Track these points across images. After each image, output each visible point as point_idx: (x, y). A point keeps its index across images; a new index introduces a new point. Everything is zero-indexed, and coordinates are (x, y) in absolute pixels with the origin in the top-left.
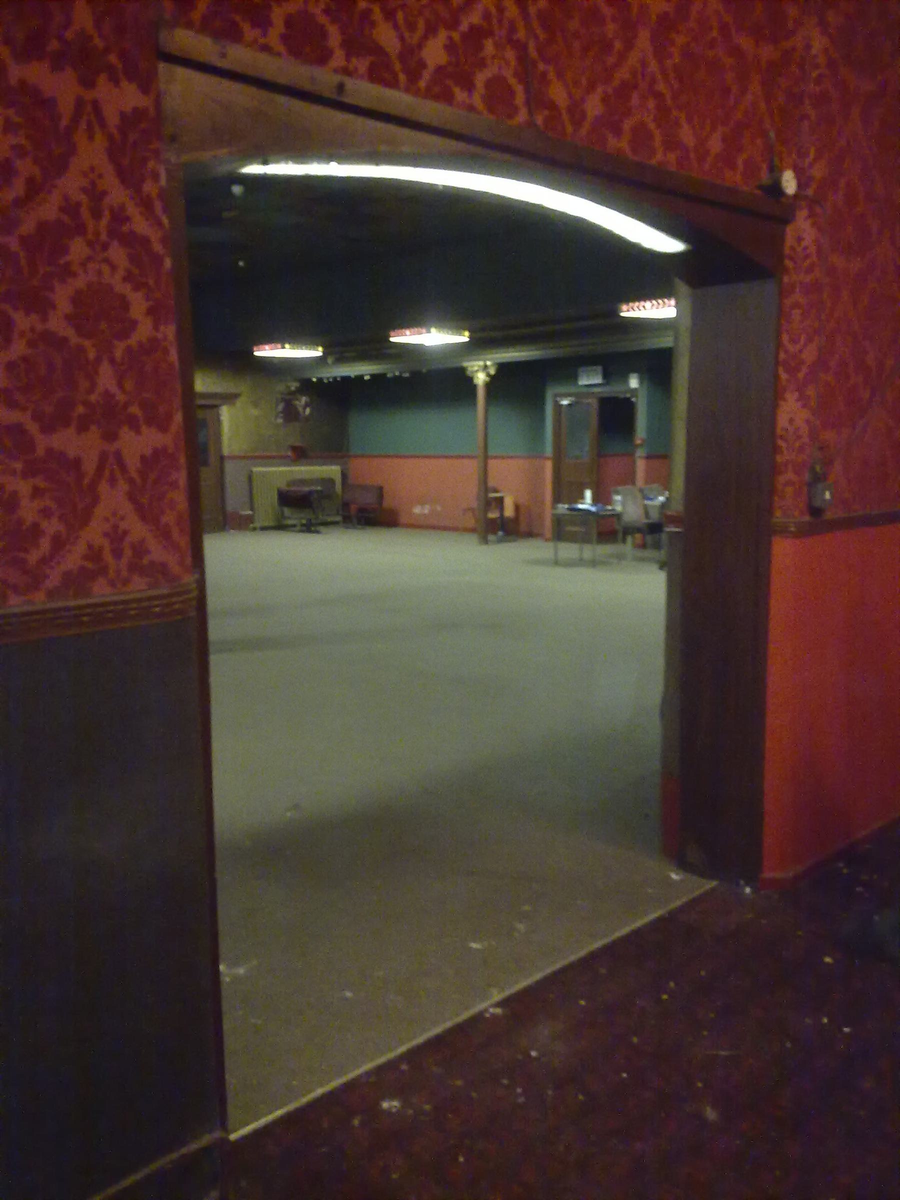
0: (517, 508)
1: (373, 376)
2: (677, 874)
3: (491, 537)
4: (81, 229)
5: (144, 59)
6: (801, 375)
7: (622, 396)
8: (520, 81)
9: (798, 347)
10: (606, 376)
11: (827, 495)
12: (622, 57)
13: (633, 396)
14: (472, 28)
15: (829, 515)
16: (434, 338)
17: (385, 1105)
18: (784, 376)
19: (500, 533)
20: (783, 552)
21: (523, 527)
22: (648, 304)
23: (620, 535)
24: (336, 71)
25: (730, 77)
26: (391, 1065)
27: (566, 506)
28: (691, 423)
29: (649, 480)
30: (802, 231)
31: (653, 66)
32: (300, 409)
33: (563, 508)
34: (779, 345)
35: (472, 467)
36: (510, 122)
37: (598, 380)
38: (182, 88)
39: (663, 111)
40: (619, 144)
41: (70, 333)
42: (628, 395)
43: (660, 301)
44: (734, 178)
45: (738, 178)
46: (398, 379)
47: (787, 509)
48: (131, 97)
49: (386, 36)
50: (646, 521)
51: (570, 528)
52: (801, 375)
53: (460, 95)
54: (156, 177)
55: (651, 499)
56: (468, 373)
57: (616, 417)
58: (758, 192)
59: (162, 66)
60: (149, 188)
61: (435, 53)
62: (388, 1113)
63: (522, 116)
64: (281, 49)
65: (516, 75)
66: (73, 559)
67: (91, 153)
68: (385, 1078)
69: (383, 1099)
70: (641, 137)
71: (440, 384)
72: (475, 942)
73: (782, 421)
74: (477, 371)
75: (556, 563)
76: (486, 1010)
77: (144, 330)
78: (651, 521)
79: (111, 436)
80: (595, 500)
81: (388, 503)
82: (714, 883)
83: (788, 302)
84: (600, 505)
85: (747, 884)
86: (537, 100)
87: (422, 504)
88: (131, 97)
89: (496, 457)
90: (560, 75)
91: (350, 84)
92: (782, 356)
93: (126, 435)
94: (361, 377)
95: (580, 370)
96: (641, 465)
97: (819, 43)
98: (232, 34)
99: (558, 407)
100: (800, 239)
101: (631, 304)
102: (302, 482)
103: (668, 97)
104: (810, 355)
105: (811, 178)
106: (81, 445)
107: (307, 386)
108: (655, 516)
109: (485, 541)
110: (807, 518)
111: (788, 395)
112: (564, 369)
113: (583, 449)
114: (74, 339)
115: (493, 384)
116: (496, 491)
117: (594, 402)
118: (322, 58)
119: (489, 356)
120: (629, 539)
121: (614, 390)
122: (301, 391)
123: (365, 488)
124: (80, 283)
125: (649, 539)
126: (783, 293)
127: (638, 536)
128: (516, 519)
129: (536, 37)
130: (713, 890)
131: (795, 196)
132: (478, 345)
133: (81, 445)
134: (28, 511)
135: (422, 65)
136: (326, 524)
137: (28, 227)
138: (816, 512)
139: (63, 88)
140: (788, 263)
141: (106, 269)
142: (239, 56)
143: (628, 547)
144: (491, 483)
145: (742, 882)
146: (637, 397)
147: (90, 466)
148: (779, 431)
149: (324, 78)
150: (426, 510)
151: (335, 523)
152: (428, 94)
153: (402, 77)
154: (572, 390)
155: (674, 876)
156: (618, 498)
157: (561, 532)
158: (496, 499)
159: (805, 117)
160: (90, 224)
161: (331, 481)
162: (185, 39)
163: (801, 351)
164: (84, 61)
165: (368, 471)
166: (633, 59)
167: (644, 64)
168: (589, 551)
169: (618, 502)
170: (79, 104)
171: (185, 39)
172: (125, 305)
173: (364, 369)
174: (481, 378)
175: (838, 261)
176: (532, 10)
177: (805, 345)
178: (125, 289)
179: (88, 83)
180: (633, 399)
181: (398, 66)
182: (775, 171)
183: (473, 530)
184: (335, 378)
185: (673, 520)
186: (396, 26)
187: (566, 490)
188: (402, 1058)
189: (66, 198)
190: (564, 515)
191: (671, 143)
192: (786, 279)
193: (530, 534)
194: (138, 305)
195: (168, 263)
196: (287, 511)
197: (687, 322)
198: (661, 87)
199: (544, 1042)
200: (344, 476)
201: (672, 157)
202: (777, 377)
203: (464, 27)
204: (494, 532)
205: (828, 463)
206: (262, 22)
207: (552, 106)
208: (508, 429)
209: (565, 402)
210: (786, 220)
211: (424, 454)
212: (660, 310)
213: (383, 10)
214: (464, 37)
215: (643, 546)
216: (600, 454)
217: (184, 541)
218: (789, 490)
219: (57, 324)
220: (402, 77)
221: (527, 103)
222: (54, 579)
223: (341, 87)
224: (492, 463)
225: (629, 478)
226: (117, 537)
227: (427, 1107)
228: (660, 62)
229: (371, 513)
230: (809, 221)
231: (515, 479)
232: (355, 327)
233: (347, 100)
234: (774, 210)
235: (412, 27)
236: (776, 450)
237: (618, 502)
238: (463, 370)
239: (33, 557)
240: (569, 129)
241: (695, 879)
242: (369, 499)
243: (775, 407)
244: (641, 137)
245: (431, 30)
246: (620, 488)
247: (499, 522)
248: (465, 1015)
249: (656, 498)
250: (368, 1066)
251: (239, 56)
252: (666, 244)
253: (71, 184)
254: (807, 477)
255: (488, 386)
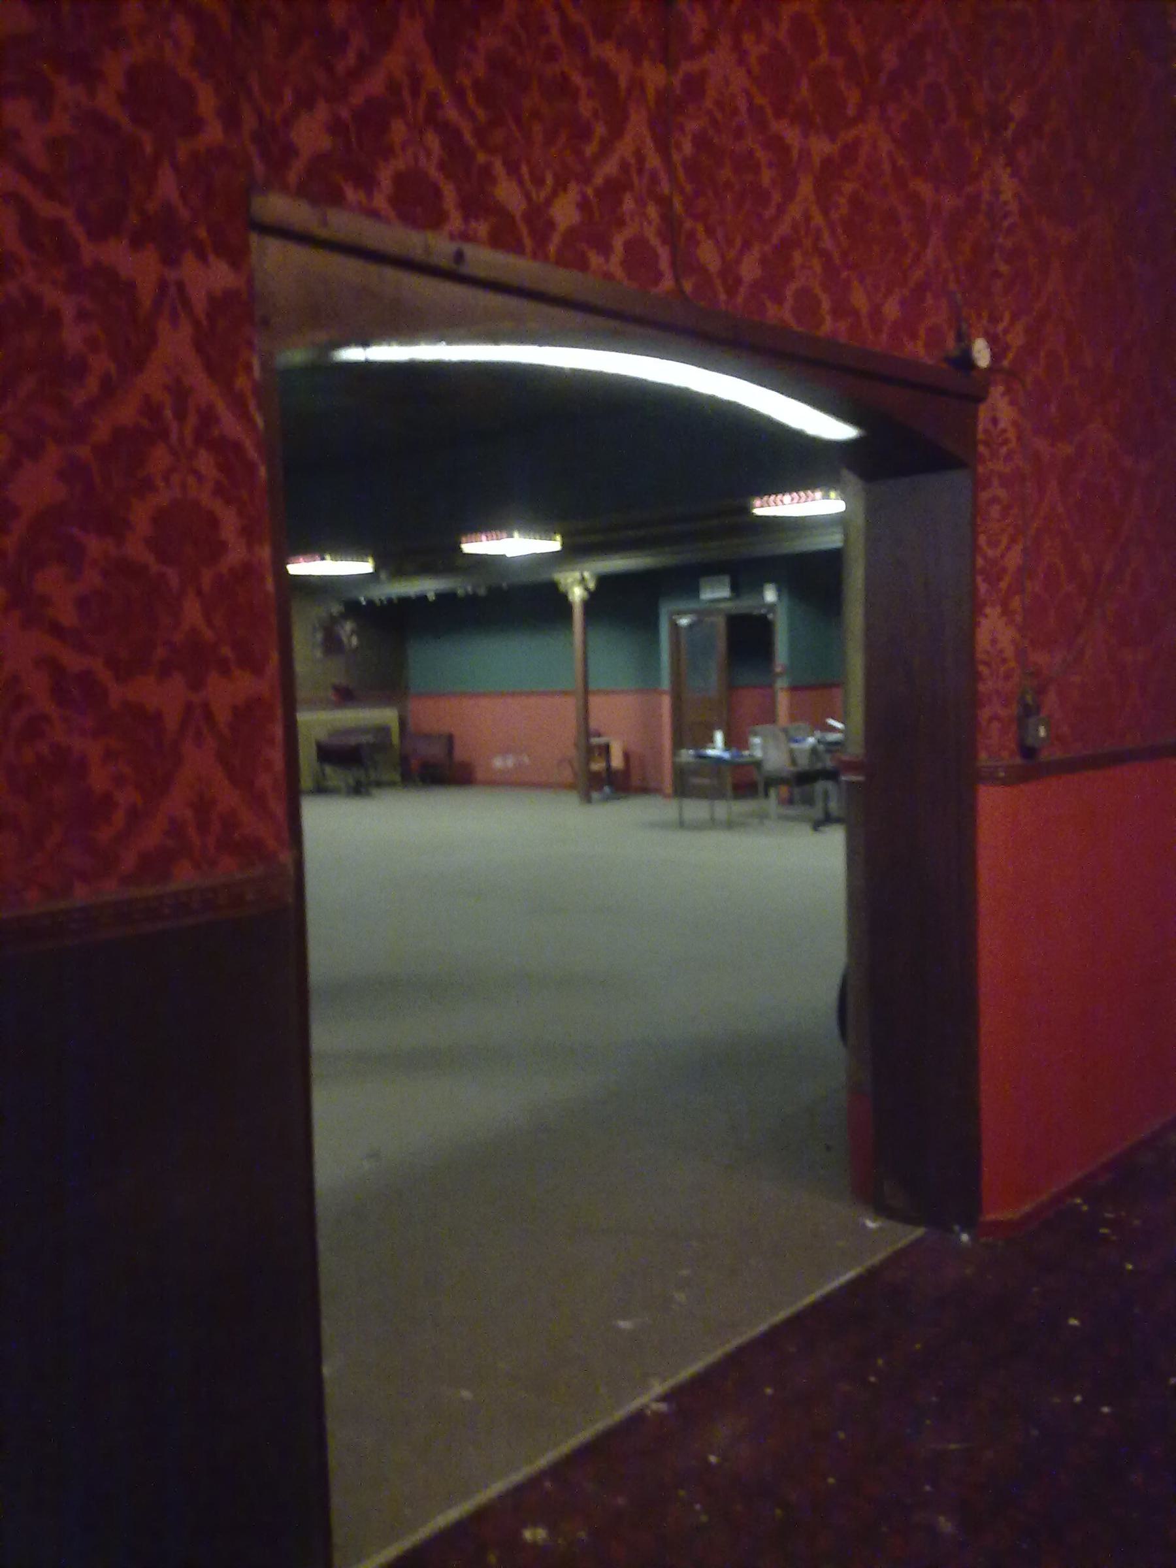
0: (627, 756)
1: (440, 596)
2: (874, 1221)
3: (595, 795)
4: (164, 434)
5: (233, 230)
6: (1003, 585)
7: (756, 612)
8: (664, 242)
9: (998, 552)
10: (736, 588)
11: (1042, 732)
12: (781, 209)
13: (769, 612)
14: (608, 181)
15: (1045, 756)
16: (516, 545)
17: (528, 1535)
18: (983, 587)
19: (607, 789)
20: (991, 800)
21: (635, 780)
22: (787, 498)
23: (761, 788)
24: (452, 237)
25: (907, 228)
26: (533, 1482)
27: (691, 752)
28: (871, 648)
29: (793, 718)
30: (999, 410)
31: (818, 219)
32: (345, 639)
33: (687, 755)
34: (975, 548)
35: (569, 707)
36: (654, 291)
37: (724, 592)
38: (274, 259)
39: (670, 229)
40: (781, 313)
41: (149, 559)
42: (763, 611)
43: (802, 494)
44: (917, 350)
45: (788, 316)
46: (472, 599)
47: (994, 748)
48: (219, 276)
49: (507, 193)
50: (792, 769)
51: (697, 781)
52: (1003, 585)
53: (595, 259)
54: (248, 368)
55: (796, 741)
56: (562, 588)
57: (748, 639)
58: (944, 366)
59: (254, 238)
60: (241, 382)
61: (565, 212)
62: (534, 1545)
63: (668, 283)
64: (392, 214)
65: (659, 233)
66: (152, 836)
67: (175, 343)
68: (522, 1502)
69: (525, 1525)
70: (806, 305)
71: (527, 601)
72: (624, 1319)
73: (983, 638)
74: (573, 584)
75: (682, 825)
76: (647, 1406)
77: (236, 554)
78: (799, 769)
79: (196, 684)
80: (728, 744)
81: (459, 754)
82: (920, 1232)
83: (985, 496)
84: (734, 750)
85: (963, 1230)
86: (685, 264)
87: (505, 751)
88: (219, 276)
89: (607, 693)
90: (710, 231)
91: (469, 250)
92: (980, 562)
93: (189, 260)
94: (422, 599)
95: (703, 581)
96: (783, 700)
97: (1009, 187)
98: (335, 198)
99: (675, 627)
100: (995, 421)
101: (766, 498)
102: (348, 732)
103: (836, 255)
104: (1014, 559)
105: (1007, 348)
106: (165, 696)
107: (353, 609)
108: (804, 763)
109: (587, 799)
110: (1018, 760)
111: (988, 610)
112: (684, 581)
113: (710, 679)
114: (155, 567)
115: (593, 603)
116: (599, 735)
117: (721, 622)
118: (435, 220)
119: (587, 565)
120: (773, 792)
121: (745, 605)
122: (344, 616)
123: (428, 736)
124: (163, 497)
125: (797, 791)
126: (979, 484)
127: (784, 790)
128: (627, 771)
129: (682, 191)
130: (919, 1241)
131: (990, 369)
132: (573, 552)
133: (165, 696)
134: (99, 779)
135: (551, 225)
136: (379, 784)
137: (102, 431)
138: (1028, 752)
139: (140, 267)
140: (981, 448)
141: (191, 480)
142: (344, 223)
143: (771, 804)
144: (593, 724)
145: (957, 1228)
146: (774, 612)
147: (171, 723)
148: (980, 656)
149: (439, 246)
150: (510, 762)
151: (391, 784)
152: (560, 262)
153: (528, 242)
154: (693, 605)
155: (871, 1224)
156: (757, 740)
157: (685, 785)
158: (600, 747)
159: (996, 274)
160: (174, 426)
161: (384, 730)
162: (277, 206)
163: (1003, 556)
164: (166, 237)
165: (432, 715)
166: (795, 211)
167: (808, 218)
168: (722, 809)
169: (758, 746)
170: (163, 286)
171: (277, 206)
172: (214, 523)
173: (427, 586)
174: (577, 594)
175: (1041, 444)
176: (676, 157)
177: (1008, 548)
178: (217, 506)
179: (170, 260)
180: (770, 616)
181: (524, 230)
182: (964, 340)
183: (571, 787)
184: (390, 600)
185: (850, 767)
186: (521, 182)
187: (689, 732)
188: (543, 1474)
189: (147, 398)
190: (689, 763)
191: (841, 309)
192: (980, 469)
193: (645, 790)
194: (230, 523)
195: (262, 471)
196: (328, 770)
197: (860, 521)
198: (827, 243)
199: (721, 1443)
200: (403, 722)
201: (843, 326)
202: (975, 589)
203: (599, 180)
204: (600, 789)
205: (1041, 691)
206: (367, 182)
207: (701, 269)
208: (612, 658)
209: (684, 621)
210: (979, 398)
211: (498, 691)
212: (821, 505)
213: (506, 163)
214: (598, 192)
215: (790, 801)
216: (731, 687)
217: (278, 809)
218: (996, 725)
219: (136, 549)
220: (528, 242)
221: (673, 264)
222: (129, 861)
223: (459, 257)
224: (594, 701)
225: (768, 716)
226: (202, 806)
227: (582, 1535)
228: (825, 212)
229: (438, 768)
230: (1006, 399)
231: (625, 717)
232: (416, 533)
233: (465, 270)
234: (962, 386)
235: (539, 182)
236: (977, 677)
237: (758, 746)
238: (553, 586)
239: (79, 397)
240: (723, 297)
241: (900, 1228)
242: (435, 751)
243: (975, 625)
244: (806, 305)
245: (561, 185)
246: (758, 728)
247: (604, 775)
248: (619, 1415)
249: (804, 739)
250: (497, 1488)
251: (344, 223)
252: (837, 430)
253: (152, 380)
254: (1015, 709)
255: (588, 605)
